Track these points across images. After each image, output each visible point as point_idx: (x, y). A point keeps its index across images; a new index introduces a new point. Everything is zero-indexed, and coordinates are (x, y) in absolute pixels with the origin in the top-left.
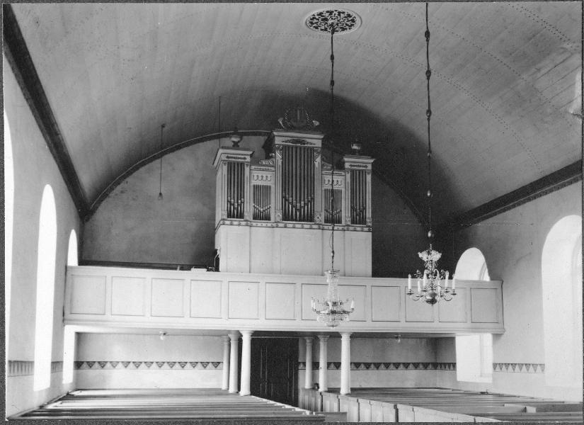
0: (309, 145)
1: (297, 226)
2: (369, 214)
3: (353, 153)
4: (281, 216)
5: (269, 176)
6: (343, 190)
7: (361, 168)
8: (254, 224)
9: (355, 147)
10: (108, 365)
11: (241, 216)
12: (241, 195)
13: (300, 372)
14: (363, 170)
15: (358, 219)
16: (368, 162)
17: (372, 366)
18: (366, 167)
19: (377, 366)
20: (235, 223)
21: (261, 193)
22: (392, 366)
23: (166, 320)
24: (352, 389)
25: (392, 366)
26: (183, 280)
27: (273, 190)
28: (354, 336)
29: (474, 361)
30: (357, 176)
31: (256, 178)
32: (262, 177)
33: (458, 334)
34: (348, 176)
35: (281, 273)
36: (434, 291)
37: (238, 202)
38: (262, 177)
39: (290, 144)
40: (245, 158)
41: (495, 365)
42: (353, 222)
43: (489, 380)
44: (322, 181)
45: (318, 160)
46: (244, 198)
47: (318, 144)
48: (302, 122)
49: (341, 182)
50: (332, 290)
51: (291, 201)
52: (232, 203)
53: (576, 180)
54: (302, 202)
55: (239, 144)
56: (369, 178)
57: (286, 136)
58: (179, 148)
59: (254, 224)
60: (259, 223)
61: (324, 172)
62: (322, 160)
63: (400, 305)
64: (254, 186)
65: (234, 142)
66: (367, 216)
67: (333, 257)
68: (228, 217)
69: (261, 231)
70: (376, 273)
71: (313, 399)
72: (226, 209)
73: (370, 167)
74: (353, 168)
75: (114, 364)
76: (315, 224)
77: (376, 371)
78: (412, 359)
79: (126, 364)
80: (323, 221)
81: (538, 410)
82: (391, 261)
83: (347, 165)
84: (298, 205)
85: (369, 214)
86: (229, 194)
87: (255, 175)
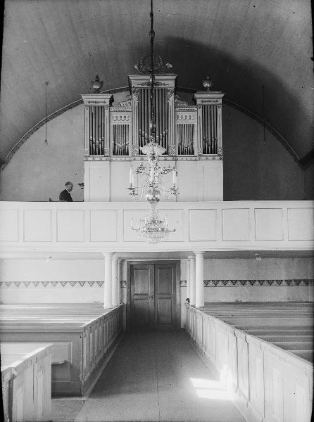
0: (163, 86)
2: (220, 143)
3: (205, 90)
6: (130, 125)
8: (114, 159)
9: (206, 85)
10: (22, 285)
11: (191, 152)
14: (213, 105)
15: (209, 149)
16: (217, 97)
17: (248, 283)
18: (217, 101)
20: (97, 159)
21: (121, 130)
22: (266, 283)
23: (239, 243)
24: (206, 304)
25: (266, 283)
27: (130, 128)
28: (208, 256)
32: (121, 117)
34: (200, 111)
38: (121, 117)
39: (145, 86)
40: (105, 102)
41: (206, 283)
44: (176, 117)
45: (172, 98)
47: (171, 84)
49: (190, 117)
51: (146, 137)
52: (94, 141)
54: (100, 139)
56: (220, 111)
59: (114, 159)
60: (119, 158)
61: (177, 109)
62: (175, 98)
70: (228, 197)
74: (204, 103)
78: (231, 276)
79: (36, 284)
82: (238, 187)
83: (199, 102)
87: (180, 115)
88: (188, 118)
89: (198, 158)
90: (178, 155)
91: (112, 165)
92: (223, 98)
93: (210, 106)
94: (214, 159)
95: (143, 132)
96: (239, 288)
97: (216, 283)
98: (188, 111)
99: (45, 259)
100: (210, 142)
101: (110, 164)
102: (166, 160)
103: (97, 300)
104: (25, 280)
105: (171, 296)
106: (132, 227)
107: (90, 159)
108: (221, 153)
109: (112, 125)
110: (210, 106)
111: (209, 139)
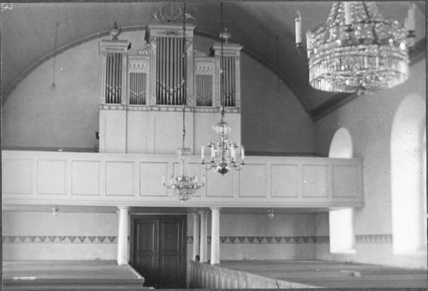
1: (170, 109)
2: (238, 96)
3: (222, 41)
4: (155, 100)
5: (145, 64)
6: (149, 73)
7: (230, 55)
8: (197, 110)
9: (225, 36)
12: (119, 82)
13: (188, 245)
18: (235, 54)
19: (260, 239)
20: (170, 109)
21: (138, 79)
25: (274, 240)
26: (100, 161)
27: (148, 77)
28: (225, 212)
29: (342, 234)
30: (227, 64)
31: (132, 66)
33: (331, 208)
34: (219, 63)
35: (155, 153)
36: (225, 162)
37: (115, 89)
42: (158, 103)
43: (353, 252)
44: (194, 67)
46: (121, 84)
48: (176, 15)
49: (210, 68)
50: (187, 168)
51: (164, 86)
52: (110, 89)
53: (421, 59)
54: (117, 87)
55: (118, 37)
56: (238, 63)
57: (161, 29)
58: (80, 43)
59: (197, 110)
62: (194, 48)
63: (290, 182)
64: (131, 74)
65: (113, 36)
66: (237, 99)
67: (184, 135)
68: (106, 102)
69: (137, 114)
71: (196, 270)
72: (220, 98)
73: (238, 54)
74: (110, 51)
75: (23, 239)
76: (236, 109)
77: (230, 245)
80: (195, 104)
81: (362, 275)
82: (256, 143)
84: (171, 90)
85: (238, 96)
86: (108, 81)
88: (206, 69)
89: (149, 108)
90: (129, 105)
91: (129, 116)
92: (242, 51)
93: (229, 58)
94: (117, 109)
95: (161, 82)
96: (77, 246)
97: (233, 239)
98: (205, 61)
99: (52, 212)
100: (228, 94)
101: (194, 116)
102: (167, 111)
103: (99, 257)
104: (50, 235)
105: (183, 253)
106: (164, 184)
107: (106, 107)
108: (239, 106)
109: (129, 72)
110: (229, 58)
111: (227, 91)
